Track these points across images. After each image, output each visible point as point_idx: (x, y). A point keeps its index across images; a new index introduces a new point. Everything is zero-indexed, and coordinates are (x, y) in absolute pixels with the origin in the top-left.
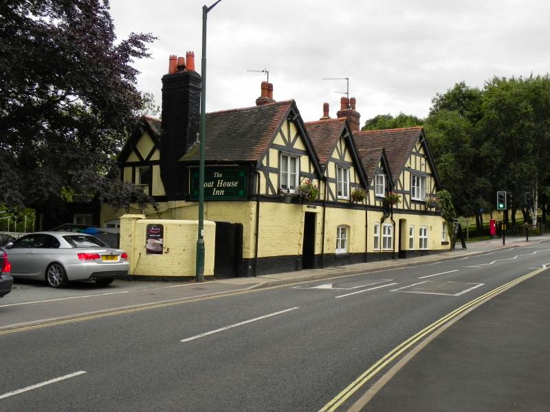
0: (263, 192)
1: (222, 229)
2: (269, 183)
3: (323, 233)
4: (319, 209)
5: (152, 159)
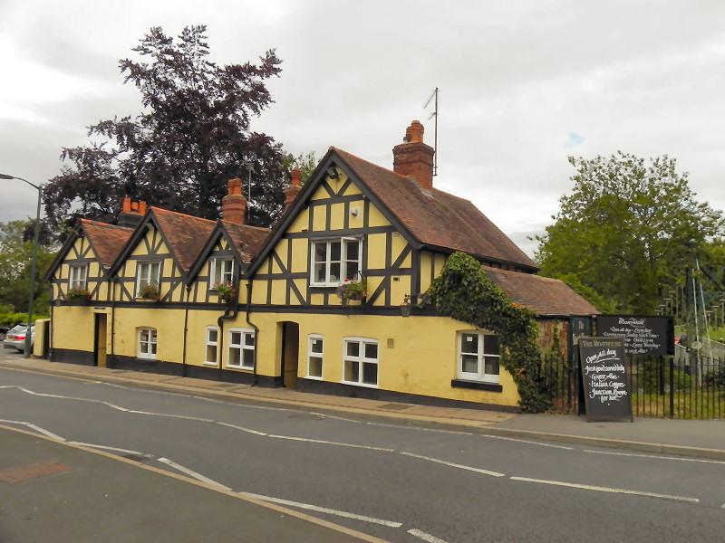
0: (55, 298)
1: (214, 360)
2: (60, 291)
3: (113, 334)
4: (108, 310)
5: (402, 266)
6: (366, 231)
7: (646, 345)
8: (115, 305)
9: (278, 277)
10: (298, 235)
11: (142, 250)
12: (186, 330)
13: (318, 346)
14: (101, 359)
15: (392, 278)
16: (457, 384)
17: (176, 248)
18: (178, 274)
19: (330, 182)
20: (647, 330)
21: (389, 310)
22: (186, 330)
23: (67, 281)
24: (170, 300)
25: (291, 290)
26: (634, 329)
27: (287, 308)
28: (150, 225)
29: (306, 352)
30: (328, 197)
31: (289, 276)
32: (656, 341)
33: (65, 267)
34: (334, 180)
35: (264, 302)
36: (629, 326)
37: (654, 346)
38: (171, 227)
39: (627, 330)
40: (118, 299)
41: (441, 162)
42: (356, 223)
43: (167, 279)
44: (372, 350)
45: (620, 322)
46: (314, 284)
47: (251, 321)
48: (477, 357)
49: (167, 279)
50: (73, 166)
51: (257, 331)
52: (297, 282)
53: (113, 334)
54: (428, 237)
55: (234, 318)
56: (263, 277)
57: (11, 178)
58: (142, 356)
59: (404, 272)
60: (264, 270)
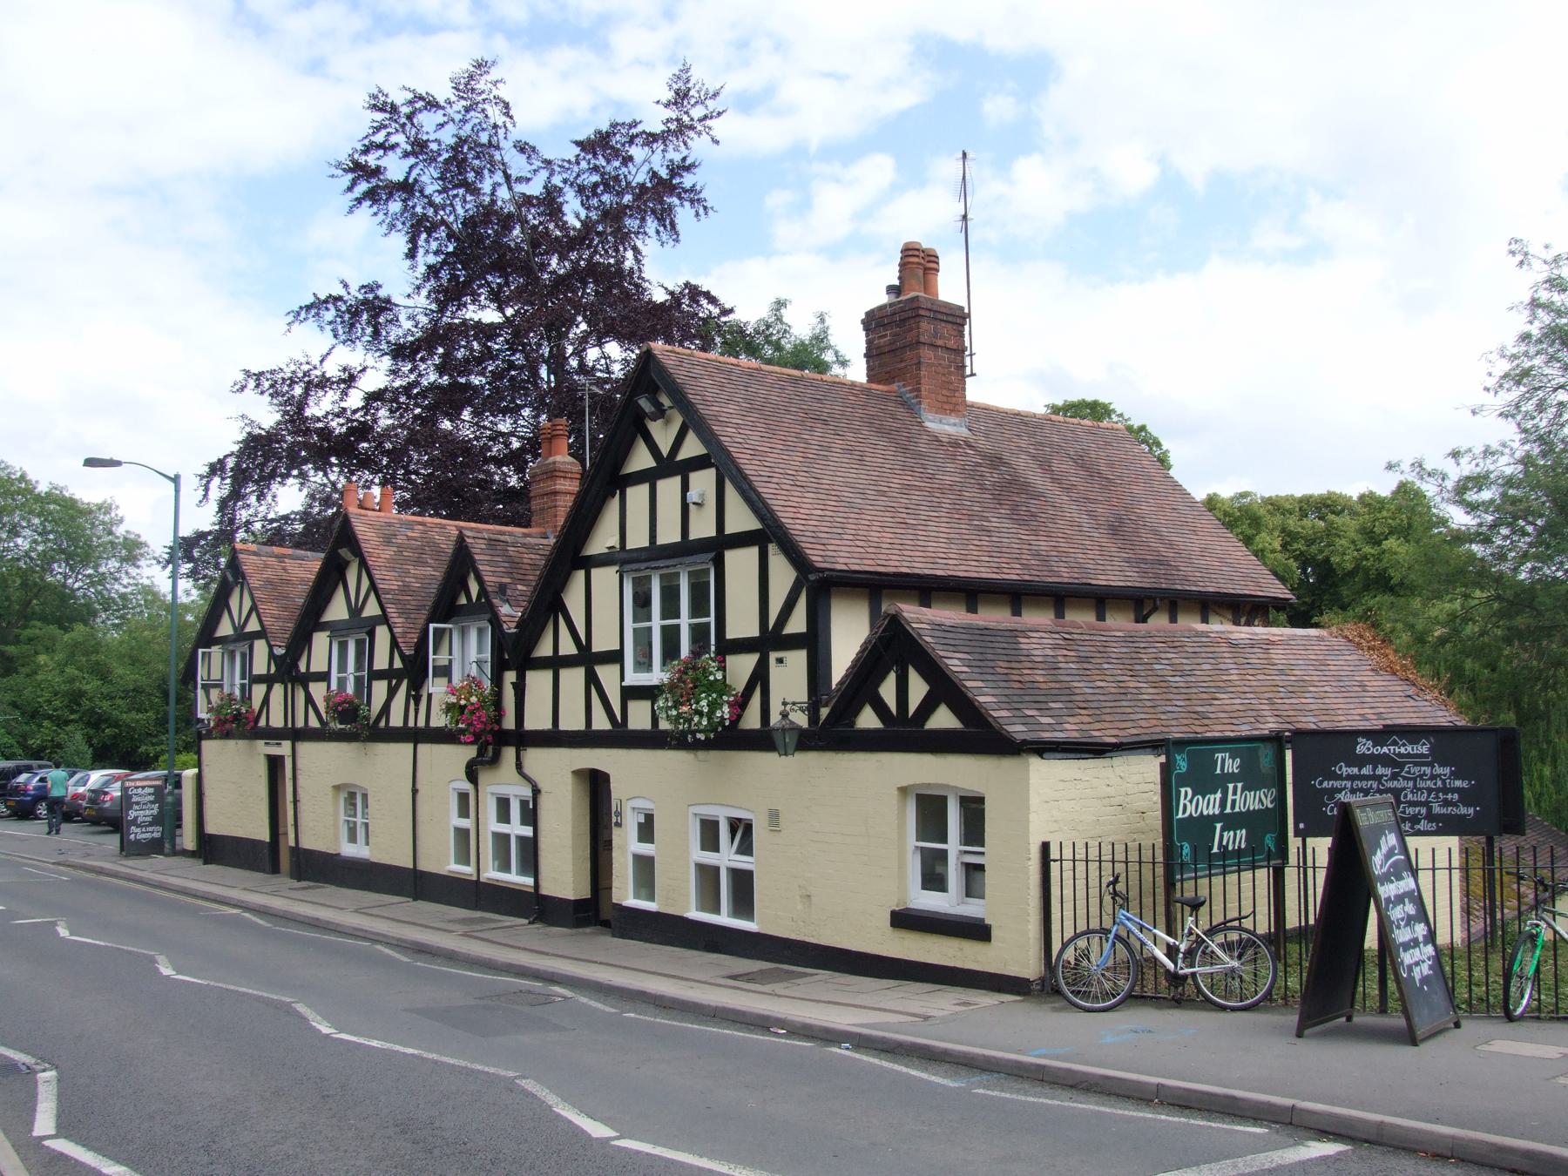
3: (295, 801)
4: (284, 749)
6: (722, 543)
7: (1437, 809)
8: (297, 735)
9: (569, 662)
10: (603, 561)
11: (337, 610)
12: (415, 791)
13: (647, 831)
14: (285, 859)
15: (773, 656)
16: (905, 920)
17: (396, 602)
18: (398, 664)
19: (655, 428)
20: (1438, 770)
21: (763, 740)
22: (415, 791)
23: (324, 677)
24: (387, 721)
25: (310, 709)
26: (1401, 766)
27: (586, 739)
28: (345, 553)
29: (626, 844)
30: (652, 463)
31: (587, 658)
32: (1466, 797)
33: (321, 640)
34: (660, 421)
35: (547, 725)
36: (1386, 760)
37: (1463, 810)
38: (389, 552)
39: (1380, 771)
40: (300, 723)
41: (981, 337)
42: (702, 527)
43: (380, 675)
44: (742, 831)
45: (1360, 749)
46: (634, 678)
47: (527, 770)
48: (945, 852)
49: (380, 675)
50: (267, 416)
51: (536, 792)
52: (607, 674)
53: (295, 801)
54: (840, 555)
55: (495, 761)
56: (543, 664)
57: (117, 463)
58: (349, 850)
59: (793, 642)
60: (545, 649)
